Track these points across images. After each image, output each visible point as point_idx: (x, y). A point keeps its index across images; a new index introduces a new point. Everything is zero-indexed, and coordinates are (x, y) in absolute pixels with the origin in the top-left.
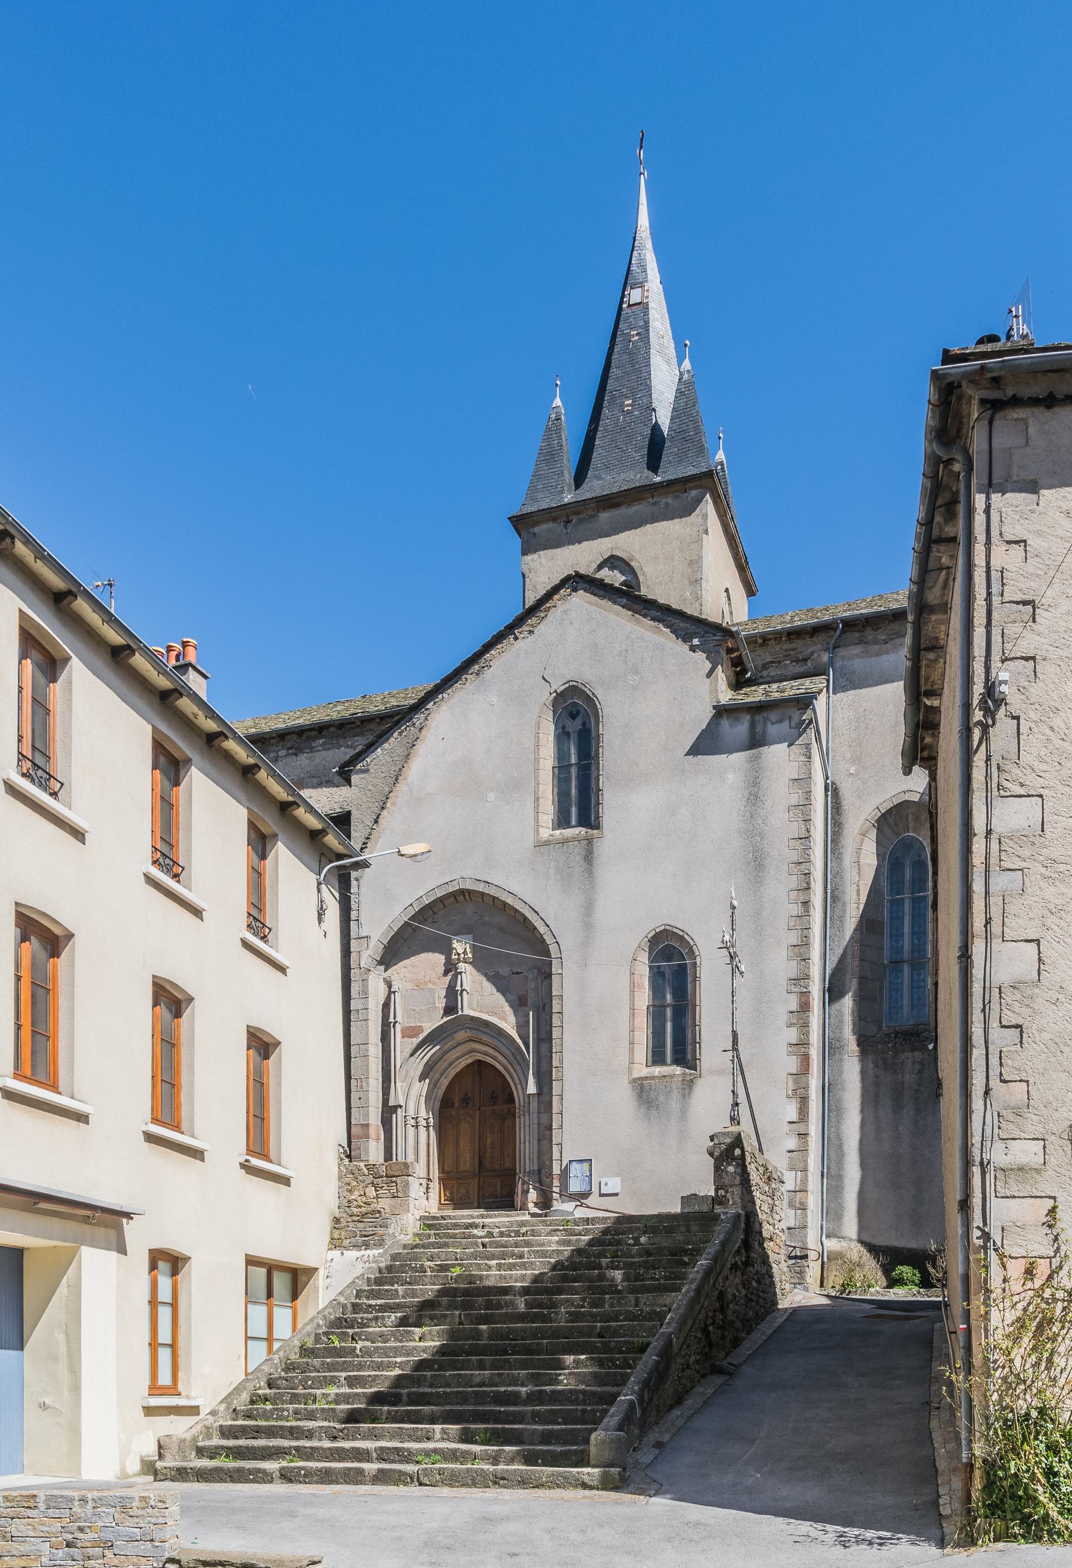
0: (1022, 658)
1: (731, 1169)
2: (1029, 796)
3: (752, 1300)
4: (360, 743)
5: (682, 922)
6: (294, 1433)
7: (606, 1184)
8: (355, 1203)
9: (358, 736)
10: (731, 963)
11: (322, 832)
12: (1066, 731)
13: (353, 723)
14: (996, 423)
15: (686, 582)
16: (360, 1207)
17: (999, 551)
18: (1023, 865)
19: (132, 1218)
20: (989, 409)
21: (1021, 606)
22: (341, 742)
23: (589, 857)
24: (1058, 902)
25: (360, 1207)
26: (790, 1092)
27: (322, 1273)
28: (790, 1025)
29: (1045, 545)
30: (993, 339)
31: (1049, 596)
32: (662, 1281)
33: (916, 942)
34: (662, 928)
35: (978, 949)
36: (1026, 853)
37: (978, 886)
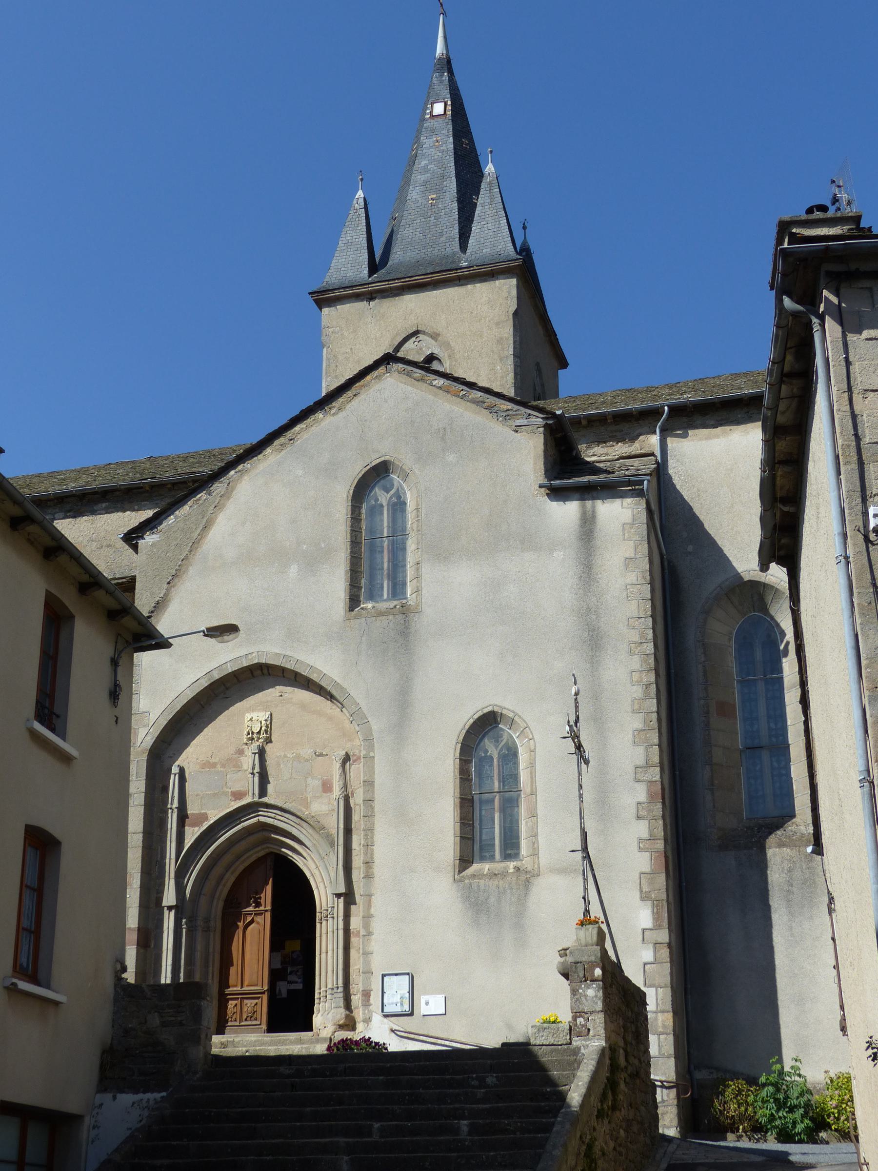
1: (591, 992)
3: (620, 1154)
7: (427, 1003)
9: (147, 501)
13: (142, 488)
15: (496, 356)
20: (833, 270)
27: (87, 1120)
28: (639, 818)
30: (823, 208)
32: (518, 1135)
33: (773, 725)
34: (490, 709)
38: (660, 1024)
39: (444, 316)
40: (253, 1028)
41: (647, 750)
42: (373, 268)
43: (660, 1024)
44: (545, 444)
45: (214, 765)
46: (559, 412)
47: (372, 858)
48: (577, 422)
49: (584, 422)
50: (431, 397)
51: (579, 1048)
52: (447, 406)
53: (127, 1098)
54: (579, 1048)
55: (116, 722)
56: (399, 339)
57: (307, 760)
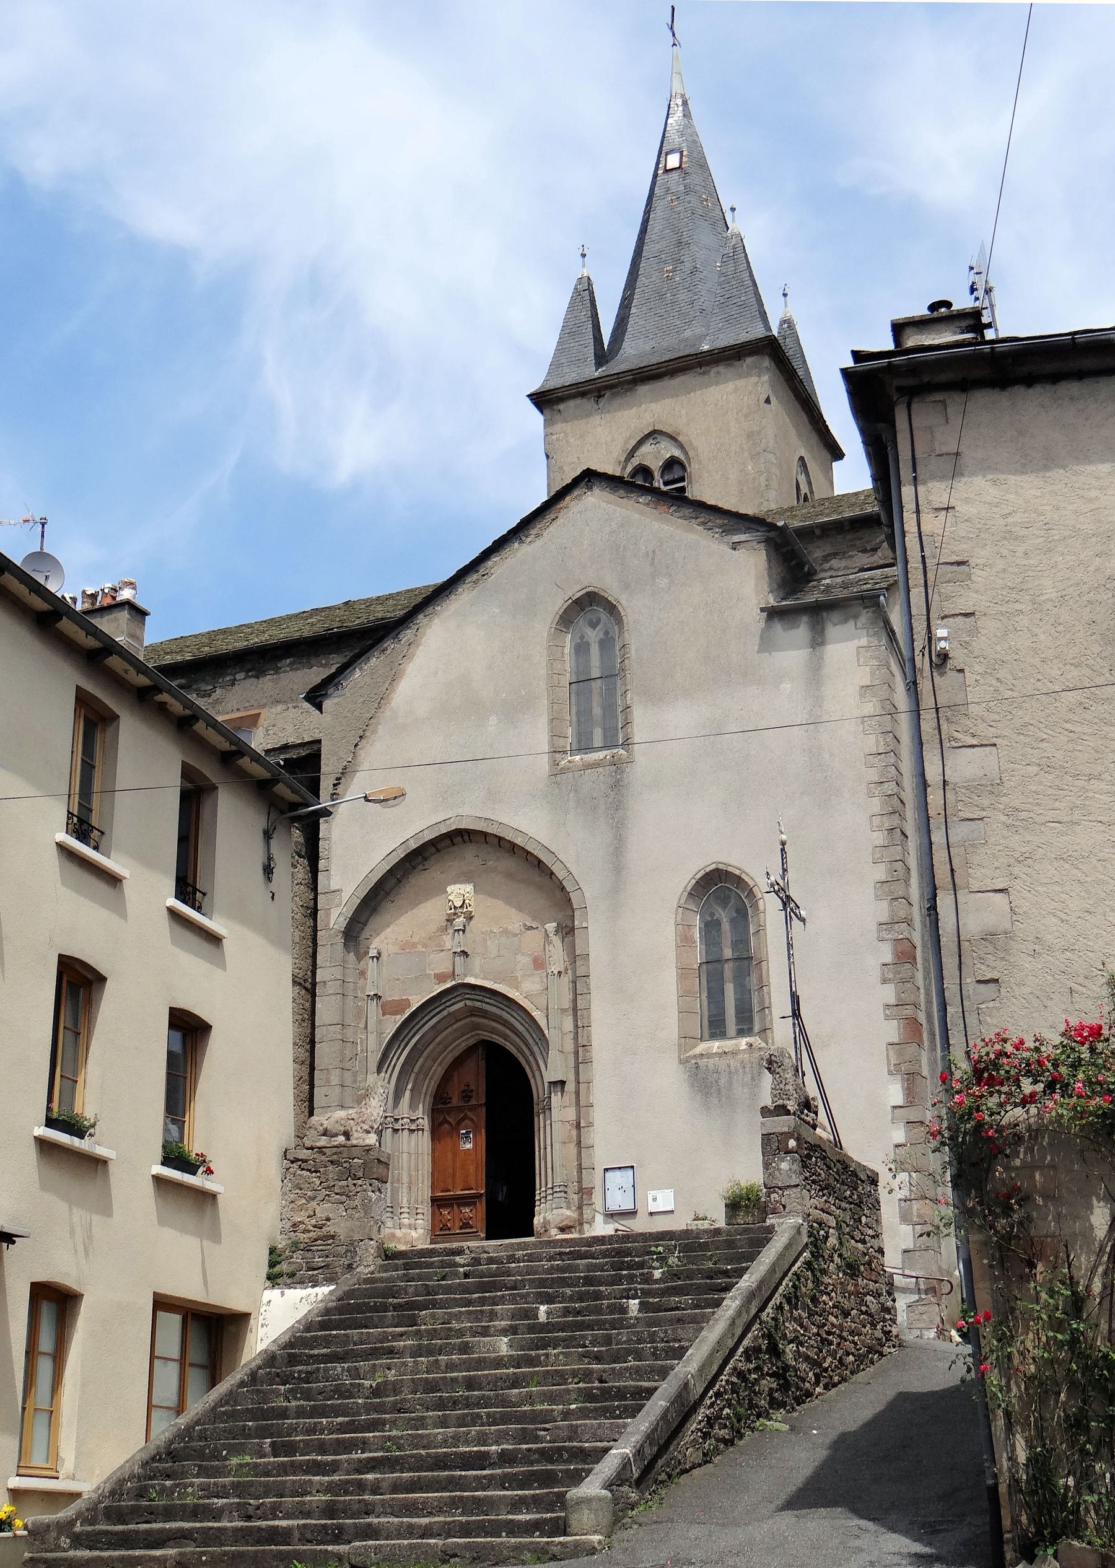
0: (961, 614)
1: (784, 1166)
2: (982, 745)
4: (335, 662)
5: (735, 860)
6: (196, 1513)
7: (655, 1200)
8: (302, 1227)
10: (785, 909)
11: (274, 781)
12: (1014, 682)
14: (914, 406)
15: (746, 454)
16: (309, 1231)
17: (927, 518)
18: (984, 814)
19: (14, 1242)
21: (955, 568)
22: (313, 661)
23: (617, 785)
24: (1023, 850)
25: (309, 1231)
26: (892, 1068)
28: (884, 981)
29: (975, 511)
31: (979, 556)
34: (713, 867)
35: (944, 902)
36: (985, 802)
37: (938, 837)
38: (915, 1213)
39: (684, 412)
40: (474, 1236)
41: (891, 905)
42: (602, 357)
43: (915, 1213)
44: (769, 561)
45: (414, 945)
46: (780, 524)
47: (589, 1041)
48: (808, 534)
49: (818, 532)
50: (637, 516)
51: (773, 1226)
52: (656, 525)
53: (295, 1294)
54: (773, 1226)
55: (273, 898)
56: (633, 442)
57: (516, 935)
